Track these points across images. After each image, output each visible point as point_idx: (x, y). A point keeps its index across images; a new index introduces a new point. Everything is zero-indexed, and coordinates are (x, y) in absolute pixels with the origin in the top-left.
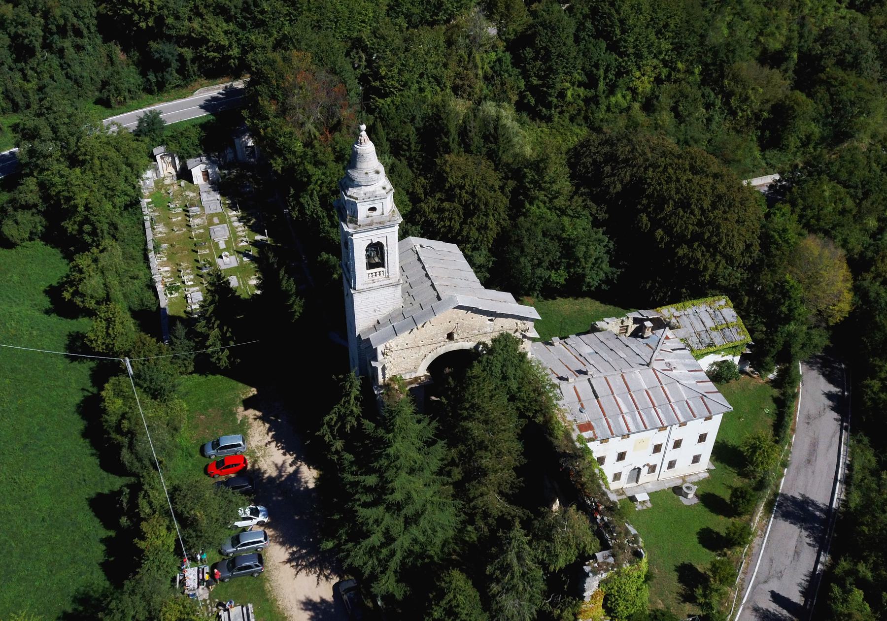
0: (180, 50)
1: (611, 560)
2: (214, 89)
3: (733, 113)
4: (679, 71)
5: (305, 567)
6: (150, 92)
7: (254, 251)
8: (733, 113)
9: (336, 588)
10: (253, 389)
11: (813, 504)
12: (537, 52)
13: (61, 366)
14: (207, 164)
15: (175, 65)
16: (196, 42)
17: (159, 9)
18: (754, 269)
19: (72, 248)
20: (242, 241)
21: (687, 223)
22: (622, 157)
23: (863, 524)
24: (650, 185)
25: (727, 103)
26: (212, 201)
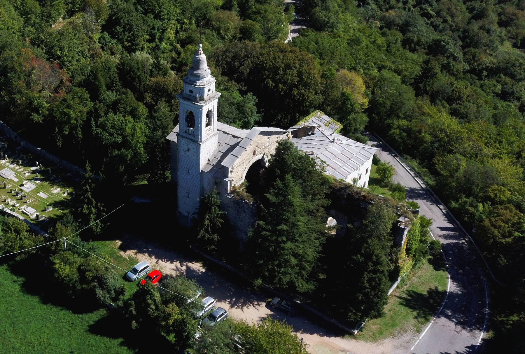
1: (407, 219)
3: (223, 38)
4: (186, 23)
5: (242, 306)
7: (39, 177)
8: (223, 38)
9: (267, 306)
10: (117, 241)
11: (416, 189)
12: (124, 27)
20: (25, 174)
21: (292, 76)
22: (242, 55)
23: (450, 183)
24: (266, 63)
25: (219, 34)
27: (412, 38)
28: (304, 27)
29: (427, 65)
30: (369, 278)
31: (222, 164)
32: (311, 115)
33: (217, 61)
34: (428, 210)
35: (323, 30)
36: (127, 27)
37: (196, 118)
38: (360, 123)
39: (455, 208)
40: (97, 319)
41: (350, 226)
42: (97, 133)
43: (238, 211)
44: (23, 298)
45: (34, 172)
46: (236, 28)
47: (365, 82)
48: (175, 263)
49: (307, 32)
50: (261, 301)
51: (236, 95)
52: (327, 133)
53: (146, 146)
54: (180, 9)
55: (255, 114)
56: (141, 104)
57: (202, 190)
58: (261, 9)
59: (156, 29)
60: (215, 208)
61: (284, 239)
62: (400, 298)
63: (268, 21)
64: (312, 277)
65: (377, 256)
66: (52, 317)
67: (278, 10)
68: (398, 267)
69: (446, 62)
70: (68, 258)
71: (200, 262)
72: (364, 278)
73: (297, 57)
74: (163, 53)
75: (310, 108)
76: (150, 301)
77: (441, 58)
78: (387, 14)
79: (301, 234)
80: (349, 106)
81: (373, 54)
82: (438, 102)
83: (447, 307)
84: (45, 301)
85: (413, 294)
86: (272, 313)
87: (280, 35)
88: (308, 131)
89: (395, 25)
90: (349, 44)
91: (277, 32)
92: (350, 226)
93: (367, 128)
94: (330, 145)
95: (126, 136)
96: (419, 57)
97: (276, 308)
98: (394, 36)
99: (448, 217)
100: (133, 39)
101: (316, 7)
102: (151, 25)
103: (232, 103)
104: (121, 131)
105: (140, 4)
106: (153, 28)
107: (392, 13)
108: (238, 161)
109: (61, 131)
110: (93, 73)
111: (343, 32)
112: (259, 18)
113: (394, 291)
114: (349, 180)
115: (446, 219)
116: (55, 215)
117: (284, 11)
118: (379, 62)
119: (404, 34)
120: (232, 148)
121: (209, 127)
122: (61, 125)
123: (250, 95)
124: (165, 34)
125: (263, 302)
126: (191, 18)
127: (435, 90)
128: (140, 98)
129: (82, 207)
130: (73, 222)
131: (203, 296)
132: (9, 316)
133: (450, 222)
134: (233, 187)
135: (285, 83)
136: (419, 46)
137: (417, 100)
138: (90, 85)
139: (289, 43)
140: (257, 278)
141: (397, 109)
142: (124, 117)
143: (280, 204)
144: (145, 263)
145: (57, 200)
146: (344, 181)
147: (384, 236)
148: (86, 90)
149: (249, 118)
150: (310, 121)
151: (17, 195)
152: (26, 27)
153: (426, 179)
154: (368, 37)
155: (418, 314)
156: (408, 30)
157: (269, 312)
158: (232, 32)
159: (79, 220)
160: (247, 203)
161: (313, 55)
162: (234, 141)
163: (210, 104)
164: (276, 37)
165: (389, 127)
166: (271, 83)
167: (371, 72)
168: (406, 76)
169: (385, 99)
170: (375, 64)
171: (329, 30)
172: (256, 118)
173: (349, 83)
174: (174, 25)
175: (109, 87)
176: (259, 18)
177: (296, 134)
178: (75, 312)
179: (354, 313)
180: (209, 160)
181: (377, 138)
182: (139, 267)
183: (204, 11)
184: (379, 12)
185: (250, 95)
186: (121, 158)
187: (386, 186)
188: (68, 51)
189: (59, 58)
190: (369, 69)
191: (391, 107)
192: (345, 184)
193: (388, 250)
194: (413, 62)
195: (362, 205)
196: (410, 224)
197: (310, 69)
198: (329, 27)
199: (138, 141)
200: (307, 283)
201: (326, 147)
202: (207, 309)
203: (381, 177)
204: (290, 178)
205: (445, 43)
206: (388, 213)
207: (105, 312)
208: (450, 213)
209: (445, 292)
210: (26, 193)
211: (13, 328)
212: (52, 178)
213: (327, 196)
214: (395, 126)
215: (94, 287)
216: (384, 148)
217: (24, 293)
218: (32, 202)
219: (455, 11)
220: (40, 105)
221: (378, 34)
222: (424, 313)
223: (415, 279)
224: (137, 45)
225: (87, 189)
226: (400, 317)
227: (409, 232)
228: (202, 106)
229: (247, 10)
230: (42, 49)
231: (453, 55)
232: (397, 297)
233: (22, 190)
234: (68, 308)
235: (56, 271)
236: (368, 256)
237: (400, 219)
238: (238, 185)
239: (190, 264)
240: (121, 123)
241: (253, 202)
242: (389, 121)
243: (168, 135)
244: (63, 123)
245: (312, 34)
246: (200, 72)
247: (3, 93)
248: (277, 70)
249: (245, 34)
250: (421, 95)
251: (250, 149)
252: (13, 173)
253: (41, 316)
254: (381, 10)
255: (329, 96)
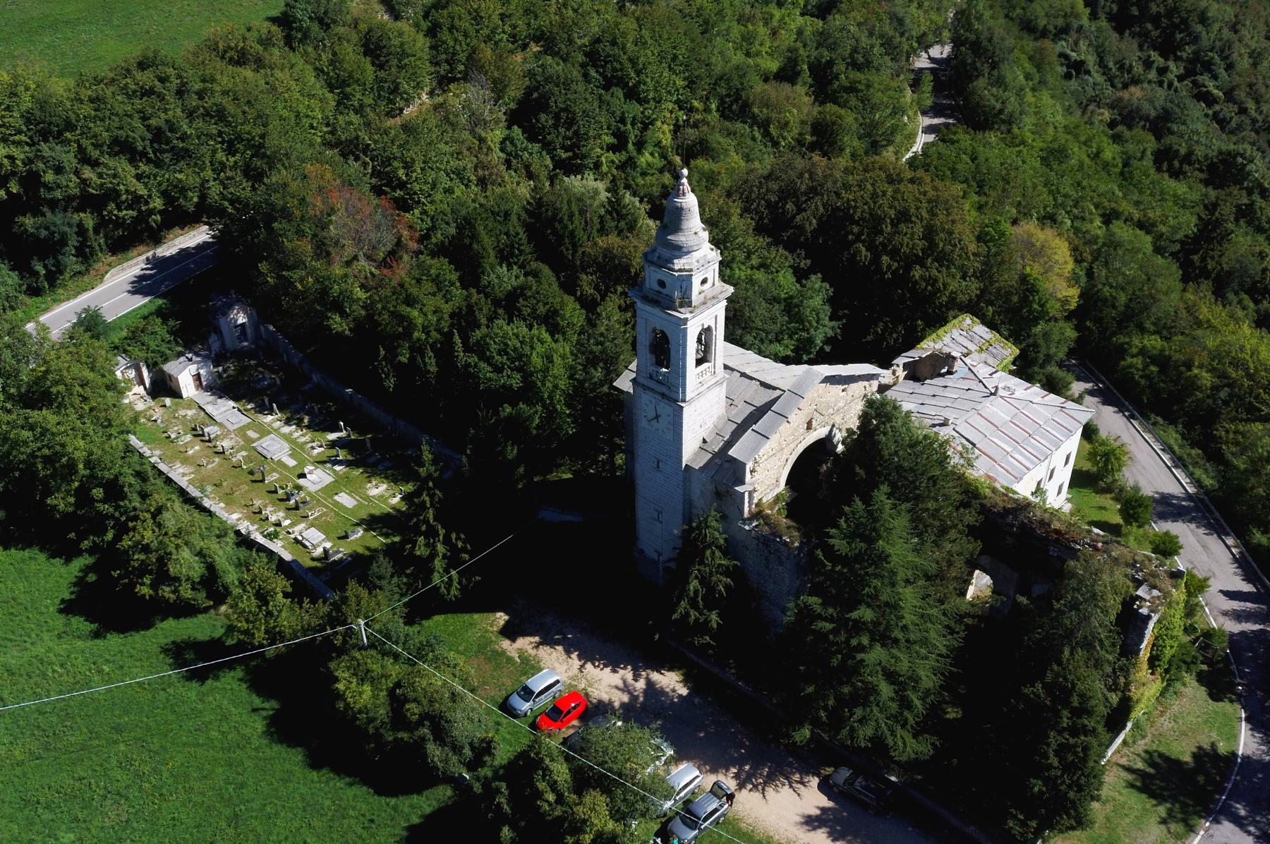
0: (76, 218)
1: (1155, 593)
2: (131, 266)
3: (776, 144)
4: (697, 110)
5: (765, 783)
6: (35, 292)
7: (342, 455)
8: (776, 144)
10: (499, 614)
11: (1173, 497)
12: (557, 117)
13: (193, 695)
14: (198, 363)
15: (73, 241)
16: (89, 201)
17: (25, 164)
18: (984, 275)
19: (72, 535)
20: (313, 448)
21: (911, 238)
22: (804, 187)
23: (1253, 488)
25: (766, 134)
26: (225, 410)
27: (1176, 147)
28: (951, 121)
29: (1212, 214)
30: (1061, 746)
31: (730, 453)
32: (949, 326)
33: (748, 200)
34: (1200, 549)
35: (991, 129)
36: (564, 115)
37: (672, 346)
38: (1058, 343)
39: (1260, 545)
40: (428, 810)
41: (1023, 600)
42: (468, 365)
43: (766, 558)
44: (268, 752)
45: (333, 444)
46: (803, 122)
47: (1074, 249)
48: (622, 672)
49: (955, 133)
50: (807, 774)
51: (787, 280)
52: (983, 371)
53: (570, 401)
54: (684, 79)
55: (826, 321)
56: (569, 300)
57: (688, 504)
58: (860, 82)
59: (629, 121)
60: (713, 553)
61: (865, 641)
62: (1129, 769)
63: (874, 108)
64: (931, 723)
65: (1082, 695)
66: (328, 803)
67: (894, 84)
68: (1129, 699)
69: (1246, 201)
70: (369, 666)
71: (679, 669)
72: (1048, 745)
73: (925, 194)
74: (644, 174)
75: (948, 309)
76: (542, 786)
77: (1235, 192)
78: (1125, 95)
79: (904, 628)
80: (1035, 306)
81: (1094, 184)
82: (1231, 296)
83: (1236, 795)
84: (315, 762)
85: (1158, 760)
86: (830, 804)
87: (898, 138)
88: (939, 365)
89: (1141, 119)
90: (1043, 159)
91: (892, 133)
92: (1023, 600)
93: (1071, 353)
94: (987, 402)
95: (532, 374)
96: (1187, 189)
97: (841, 792)
98: (1139, 142)
99: (1245, 565)
100: (576, 143)
101: (977, 77)
102: (618, 113)
103: (774, 299)
104: (520, 362)
105: (595, 66)
106: (622, 120)
107: (1135, 94)
108: (768, 447)
109: (392, 354)
110: (466, 225)
111: (1033, 133)
112: (853, 101)
113: (1118, 751)
114: (1024, 489)
115: (1239, 571)
116: (368, 549)
117: (911, 86)
118: (1107, 204)
119: (1158, 138)
120: (759, 413)
121: (705, 365)
122: (391, 343)
123: (815, 281)
124: (649, 132)
125: (814, 774)
126: (708, 99)
127: (1226, 267)
128: (569, 287)
129: (414, 543)
130: (392, 576)
131: (677, 759)
132: (230, 799)
133: (1248, 578)
134: (757, 505)
135: (894, 253)
136: (1190, 164)
137: (1184, 290)
138: (462, 253)
139: (912, 162)
140: (802, 725)
141: (1141, 312)
142: (530, 327)
143: (859, 558)
144: (556, 669)
145: (377, 512)
146: (1015, 492)
147: (1101, 641)
148: (450, 263)
149: (812, 332)
150: (947, 340)
151: (288, 499)
152: (341, 113)
153: (1198, 473)
154: (1085, 143)
155: (1170, 812)
156: (1169, 129)
157: (825, 802)
158: (796, 131)
159: (408, 572)
160: (785, 543)
161: (965, 186)
162: (764, 397)
163: (706, 311)
164: (890, 142)
165: (1122, 351)
166: (864, 253)
167: (1089, 226)
168: (1162, 235)
169: (1116, 288)
170: (1097, 207)
171: (1003, 128)
172: (827, 330)
173: (1038, 253)
174: (671, 112)
175: (506, 256)
176: (853, 101)
177: (916, 373)
178: (380, 792)
179: (1019, 820)
180: (704, 441)
181: (1092, 373)
182: (537, 683)
183: (736, 82)
184: (1109, 91)
185: (815, 281)
186: (516, 427)
187: (1107, 490)
188: (422, 169)
189: (402, 185)
190: (1083, 219)
191: (1127, 306)
192: (1016, 501)
193: (1109, 670)
194: (1179, 203)
195: (1053, 551)
196: (1162, 604)
197: (953, 222)
198: (1004, 122)
199: (556, 386)
200: (915, 736)
201: (978, 407)
202: (682, 794)
203: (1095, 472)
204: (883, 498)
205: (1244, 158)
206: (1113, 581)
207: (449, 793)
208: (1250, 559)
209: (1234, 755)
210: (309, 494)
211: (236, 828)
212: (372, 460)
213: (972, 531)
214: (1134, 350)
215: (423, 739)
216: (1107, 398)
217: (272, 740)
218: (321, 516)
219: (1263, 90)
220: (347, 296)
221: (1105, 139)
222: (1184, 807)
223: (1165, 723)
224: (584, 157)
225: (424, 502)
226: (1127, 821)
227: (1159, 621)
228: (686, 320)
229: (830, 83)
230: (365, 165)
231: (1260, 186)
232: (1123, 767)
233: (299, 488)
234: (366, 782)
235: (340, 696)
236: (1062, 693)
237: (1140, 592)
238: (768, 498)
239: (655, 676)
240: (522, 343)
241: (801, 543)
242: (1122, 339)
243: (618, 376)
244: (399, 336)
245: (965, 138)
246: (683, 239)
247: (263, 267)
248: (880, 224)
249: (823, 137)
250: (1196, 279)
251: (797, 419)
252: (286, 446)
253: (303, 800)
254: (1113, 86)
255: (991, 283)
